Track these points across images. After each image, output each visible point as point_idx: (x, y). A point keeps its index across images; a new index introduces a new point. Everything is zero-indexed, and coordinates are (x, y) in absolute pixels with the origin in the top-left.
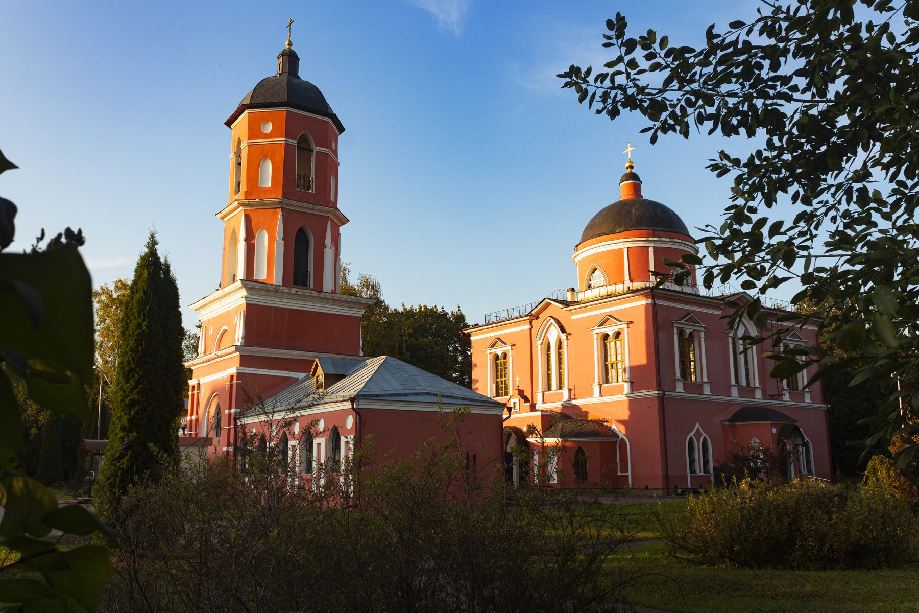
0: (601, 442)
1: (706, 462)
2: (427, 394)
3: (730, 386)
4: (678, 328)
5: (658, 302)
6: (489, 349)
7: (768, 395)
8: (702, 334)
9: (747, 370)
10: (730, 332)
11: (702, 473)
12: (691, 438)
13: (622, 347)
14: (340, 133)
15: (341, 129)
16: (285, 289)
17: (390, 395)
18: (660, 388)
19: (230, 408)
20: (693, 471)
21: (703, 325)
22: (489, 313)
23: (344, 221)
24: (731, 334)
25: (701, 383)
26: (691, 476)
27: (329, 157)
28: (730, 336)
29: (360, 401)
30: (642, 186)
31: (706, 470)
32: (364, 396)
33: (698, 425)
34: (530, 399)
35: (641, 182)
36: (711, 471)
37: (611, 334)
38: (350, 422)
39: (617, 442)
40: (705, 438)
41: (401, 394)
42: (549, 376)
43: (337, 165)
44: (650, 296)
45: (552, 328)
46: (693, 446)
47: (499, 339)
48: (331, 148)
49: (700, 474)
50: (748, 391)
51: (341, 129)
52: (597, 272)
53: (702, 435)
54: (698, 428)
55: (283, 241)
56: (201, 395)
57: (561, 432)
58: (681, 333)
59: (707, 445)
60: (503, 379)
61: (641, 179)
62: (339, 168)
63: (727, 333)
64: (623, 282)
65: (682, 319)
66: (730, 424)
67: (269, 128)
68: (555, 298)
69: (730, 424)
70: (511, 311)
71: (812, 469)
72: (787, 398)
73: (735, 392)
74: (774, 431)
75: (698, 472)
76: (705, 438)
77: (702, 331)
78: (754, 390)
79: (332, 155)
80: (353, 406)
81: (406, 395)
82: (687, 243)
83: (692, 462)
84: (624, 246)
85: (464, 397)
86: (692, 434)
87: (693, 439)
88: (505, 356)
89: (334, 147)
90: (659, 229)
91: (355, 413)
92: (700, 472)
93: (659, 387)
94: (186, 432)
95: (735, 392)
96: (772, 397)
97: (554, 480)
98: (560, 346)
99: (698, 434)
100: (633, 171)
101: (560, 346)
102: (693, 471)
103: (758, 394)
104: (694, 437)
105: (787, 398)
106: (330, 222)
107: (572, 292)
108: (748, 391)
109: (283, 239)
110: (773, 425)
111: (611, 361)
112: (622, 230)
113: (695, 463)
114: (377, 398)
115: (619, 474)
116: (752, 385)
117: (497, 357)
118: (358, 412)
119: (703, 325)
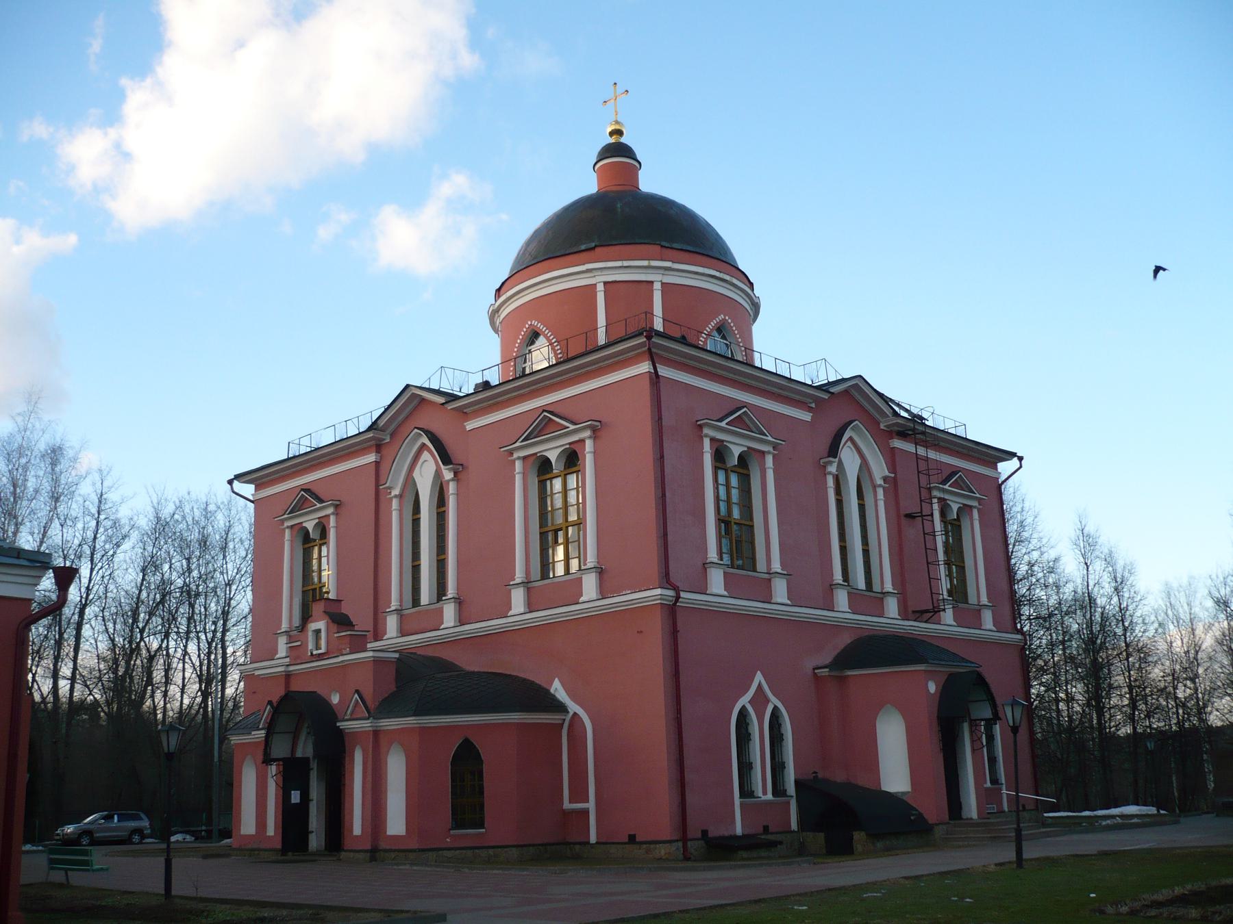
0: (521, 726)
1: (778, 768)
3: (832, 587)
4: (713, 440)
5: (664, 371)
6: (286, 516)
7: (910, 610)
8: (769, 461)
9: (866, 552)
10: (831, 463)
11: (770, 796)
12: (744, 708)
13: (581, 488)
18: (668, 582)
20: (746, 792)
21: (770, 438)
22: (294, 437)
24: (833, 469)
25: (766, 576)
26: (741, 804)
28: (830, 473)
31: (778, 790)
33: (759, 677)
35: (640, 163)
36: (791, 789)
37: (553, 456)
40: (775, 708)
42: (416, 569)
44: (647, 355)
45: (426, 455)
46: (747, 729)
47: (306, 490)
49: (764, 798)
50: (868, 600)
52: (541, 341)
53: (768, 701)
54: (760, 686)
58: (720, 455)
59: (780, 725)
63: (825, 467)
65: (721, 420)
66: (833, 674)
69: (833, 674)
71: (998, 777)
72: (948, 616)
73: (842, 599)
74: (932, 687)
75: (760, 794)
76: (775, 708)
77: (769, 452)
78: (882, 599)
82: (735, 281)
83: (745, 767)
84: (599, 280)
86: (744, 700)
87: (743, 468)
90: (675, 245)
92: (765, 793)
93: (666, 580)
95: (842, 599)
96: (919, 615)
97: (396, 824)
98: (441, 501)
99: (760, 700)
100: (623, 140)
101: (441, 501)
102: (746, 792)
103: (892, 606)
104: (750, 709)
105: (948, 616)
108: (868, 600)
110: (930, 675)
111: (552, 524)
112: (593, 245)
113: (753, 773)
115: (567, 805)
116: (877, 588)
119: (770, 438)
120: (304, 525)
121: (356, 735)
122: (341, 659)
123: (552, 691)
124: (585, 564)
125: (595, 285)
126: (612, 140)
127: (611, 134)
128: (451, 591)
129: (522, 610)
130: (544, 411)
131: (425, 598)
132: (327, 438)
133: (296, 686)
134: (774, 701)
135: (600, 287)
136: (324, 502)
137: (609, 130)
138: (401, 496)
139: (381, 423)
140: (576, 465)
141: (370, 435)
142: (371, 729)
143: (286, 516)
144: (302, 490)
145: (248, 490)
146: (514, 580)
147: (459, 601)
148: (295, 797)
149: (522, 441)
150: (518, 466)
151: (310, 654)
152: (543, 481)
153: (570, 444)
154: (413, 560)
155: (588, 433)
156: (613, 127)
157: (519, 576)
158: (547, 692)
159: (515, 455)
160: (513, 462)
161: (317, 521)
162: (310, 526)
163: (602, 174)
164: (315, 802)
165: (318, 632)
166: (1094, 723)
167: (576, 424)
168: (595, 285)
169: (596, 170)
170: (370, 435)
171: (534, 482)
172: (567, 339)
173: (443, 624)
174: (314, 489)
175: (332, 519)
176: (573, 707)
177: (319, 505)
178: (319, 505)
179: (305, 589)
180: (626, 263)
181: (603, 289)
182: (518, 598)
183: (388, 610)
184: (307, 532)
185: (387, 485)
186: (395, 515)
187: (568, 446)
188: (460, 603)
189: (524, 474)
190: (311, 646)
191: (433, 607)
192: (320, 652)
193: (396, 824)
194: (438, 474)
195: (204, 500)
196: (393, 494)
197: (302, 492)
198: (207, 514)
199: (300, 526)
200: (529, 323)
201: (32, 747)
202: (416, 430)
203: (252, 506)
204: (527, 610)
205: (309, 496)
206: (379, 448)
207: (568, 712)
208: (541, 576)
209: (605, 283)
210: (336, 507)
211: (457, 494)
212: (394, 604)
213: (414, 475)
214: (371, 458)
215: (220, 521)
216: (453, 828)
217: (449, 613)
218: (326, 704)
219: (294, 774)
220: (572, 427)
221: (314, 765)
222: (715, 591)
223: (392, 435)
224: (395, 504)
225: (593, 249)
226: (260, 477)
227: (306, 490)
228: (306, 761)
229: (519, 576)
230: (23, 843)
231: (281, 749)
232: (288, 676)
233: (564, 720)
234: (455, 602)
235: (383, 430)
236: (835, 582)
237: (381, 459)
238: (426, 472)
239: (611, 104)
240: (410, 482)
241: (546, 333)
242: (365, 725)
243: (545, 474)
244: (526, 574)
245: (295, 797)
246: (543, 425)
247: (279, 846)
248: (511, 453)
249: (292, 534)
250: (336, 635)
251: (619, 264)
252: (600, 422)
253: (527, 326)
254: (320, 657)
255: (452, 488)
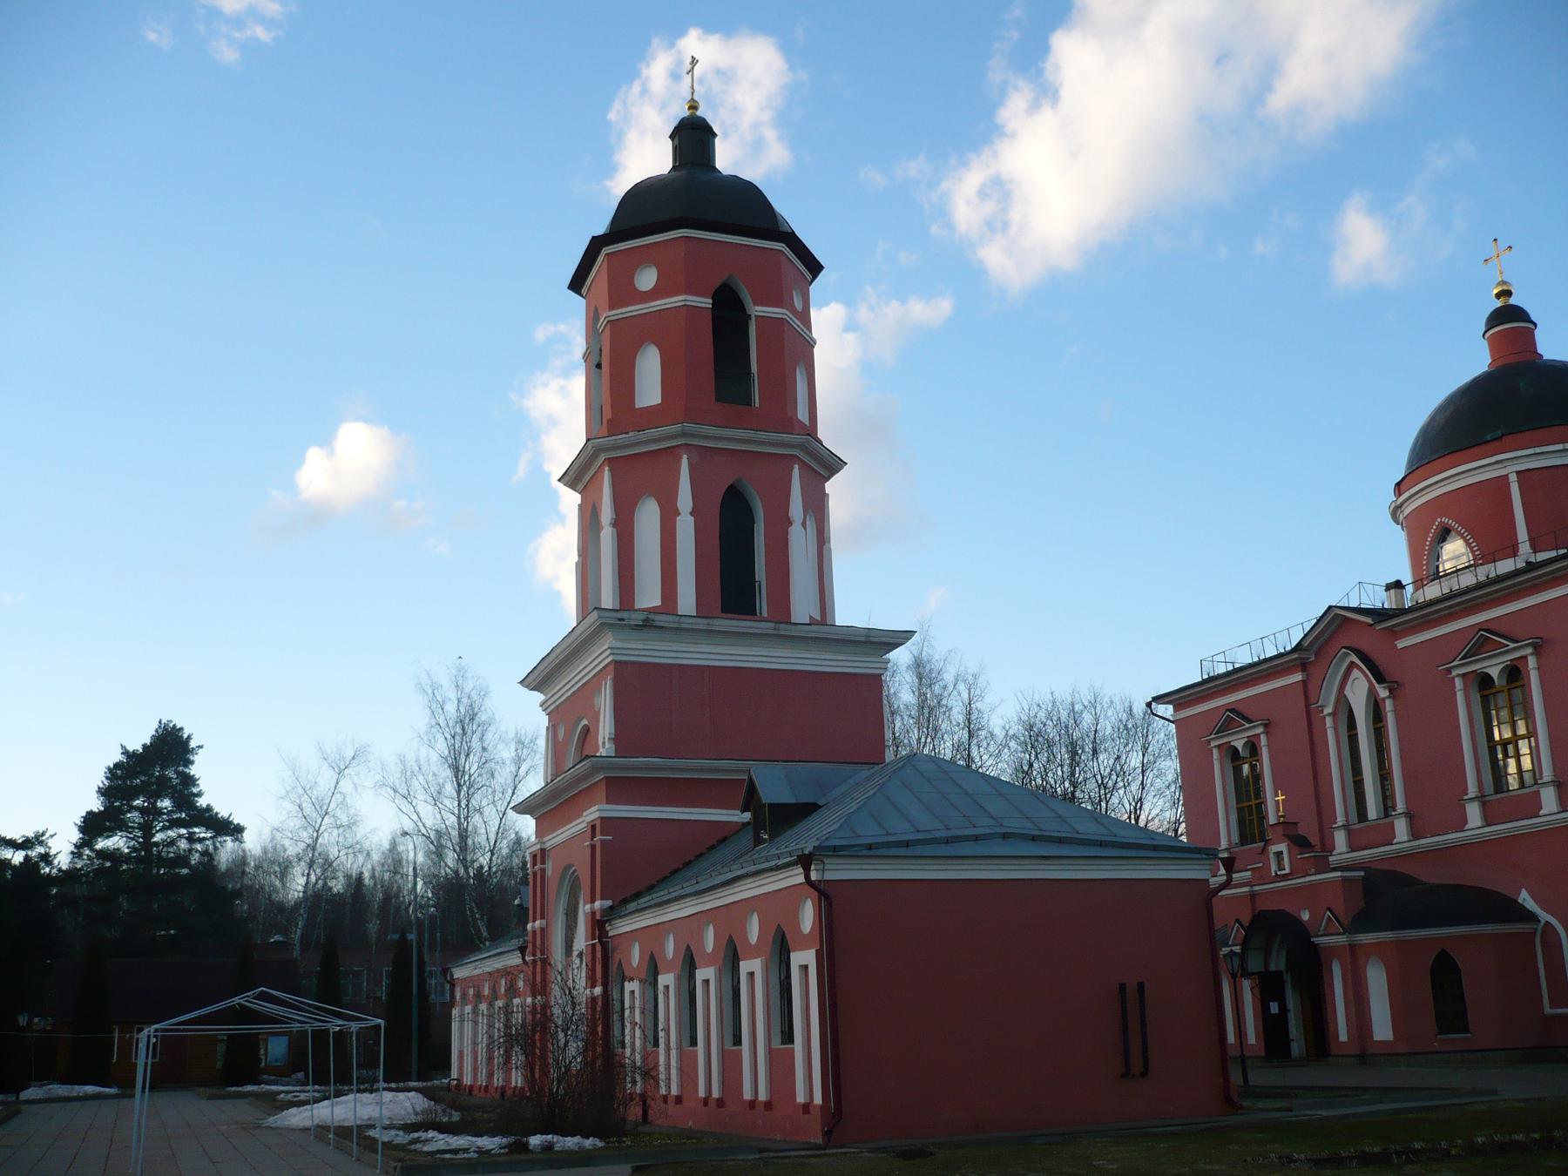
2: (1005, 836)
6: (1213, 736)
14: (815, 276)
15: (815, 267)
16: (702, 624)
17: (907, 844)
19: (593, 901)
22: (1207, 654)
23: (833, 465)
27: (786, 325)
29: (826, 861)
30: (1538, 334)
32: (835, 848)
34: (1315, 840)
35: (1535, 325)
37: (1494, 673)
38: (808, 917)
39: (1534, 933)
41: (936, 838)
43: (810, 344)
45: (1356, 673)
47: (1232, 711)
48: (793, 310)
51: (815, 267)
55: (693, 518)
56: (549, 872)
57: (459, 828)
60: (1253, 802)
61: (1534, 318)
62: (816, 350)
64: (1514, 553)
67: (647, 279)
68: (1354, 604)
70: (1257, 646)
79: (796, 322)
80: (807, 877)
81: (948, 841)
85: (1103, 838)
88: (1253, 747)
89: (798, 304)
91: (816, 893)
94: (527, 958)
97: (1382, 1029)
100: (1513, 301)
106: (796, 466)
107: (1398, 591)
109: (691, 514)
112: (1499, 433)
114: (908, 852)
115: (1548, 1010)
117: (1234, 755)
118: (824, 893)
120: (1232, 744)
121: (1333, 951)
122: (1308, 879)
123: (1520, 901)
124: (1542, 778)
125: (1507, 475)
126: (1499, 303)
127: (1498, 296)
128: (1400, 806)
129: (1479, 824)
130: (1481, 630)
131: (1372, 813)
132: (1244, 658)
133: (1263, 906)
135: (1513, 478)
136: (1252, 722)
137: (1495, 291)
138: (1334, 714)
139: (1306, 644)
140: (1517, 680)
141: (1295, 656)
142: (1346, 943)
143: (1213, 736)
144: (1228, 710)
145: (1166, 710)
146: (1467, 794)
147: (1410, 816)
148: (1274, 1008)
149: (1461, 660)
150: (1458, 683)
151: (1273, 874)
152: (1485, 696)
153: (1511, 660)
154: (1354, 776)
155: (1529, 650)
156: (1499, 289)
157: (1472, 790)
158: (1516, 902)
159: (1454, 673)
160: (1453, 679)
161: (1246, 740)
162: (1239, 745)
163: (1496, 344)
164: (1292, 1012)
165: (1279, 854)
166: (435, 1082)
167: (1517, 642)
168: (1506, 476)
169: (1486, 337)
170: (1295, 656)
171: (1476, 697)
172: (1493, 553)
173: (1395, 838)
174: (1240, 708)
175: (1263, 738)
176: (1545, 916)
177: (1247, 725)
178: (1247, 725)
179: (1240, 806)
180: (1538, 450)
181: (1516, 479)
182: (1474, 813)
183: (1334, 826)
185: (1319, 704)
186: (1330, 733)
187: (1509, 663)
188: (1410, 818)
189: (1466, 691)
190: (1274, 868)
191: (1381, 821)
192: (1283, 872)
193: (1382, 1029)
194: (1372, 692)
195: (1070, 700)
196: (1326, 712)
197: (1228, 713)
198: (1075, 716)
199: (1228, 745)
200: (1439, 520)
202: (1343, 650)
203: (1172, 726)
204: (1485, 824)
205: (1235, 717)
206: (1304, 666)
207: (1539, 921)
208: (1495, 790)
209: (1518, 473)
210: (1266, 726)
211: (1395, 711)
212: (1340, 820)
213: (666, 173)
215: (1087, 719)
216: (1439, 1034)
217: (1401, 828)
218: (1298, 921)
219: (1269, 987)
220: (1513, 645)
221: (1288, 978)
223: (1317, 654)
224: (1329, 721)
225: (1500, 438)
226: (1180, 698)
227: (1232, 711)
228: (1279, 974)
229: (1472, 790)
230: (722, 1098)
231: (1255, 964)
232: (1253, 896)
233: (1536, 929)
234: (1405, 817)
235: (1307, 649)
237: (1307, 678)
238: (1359, 690)
239: (1495, 262)
240: (1342, 701)
241: (1459, 529)
242: (1342, 939)
243: (1486, 689)
244: (1479, 788)
245: (1274, 1008)
246: (1482, 642)
247: (1263, 1054)
248: (1449, 671)
249: (1220, 755)
250: (1299, 857)
251: (1531, 451)
252: (1541, 638)
253: (1437, 523)
254: (1285, 877)
255: (1389, 705)
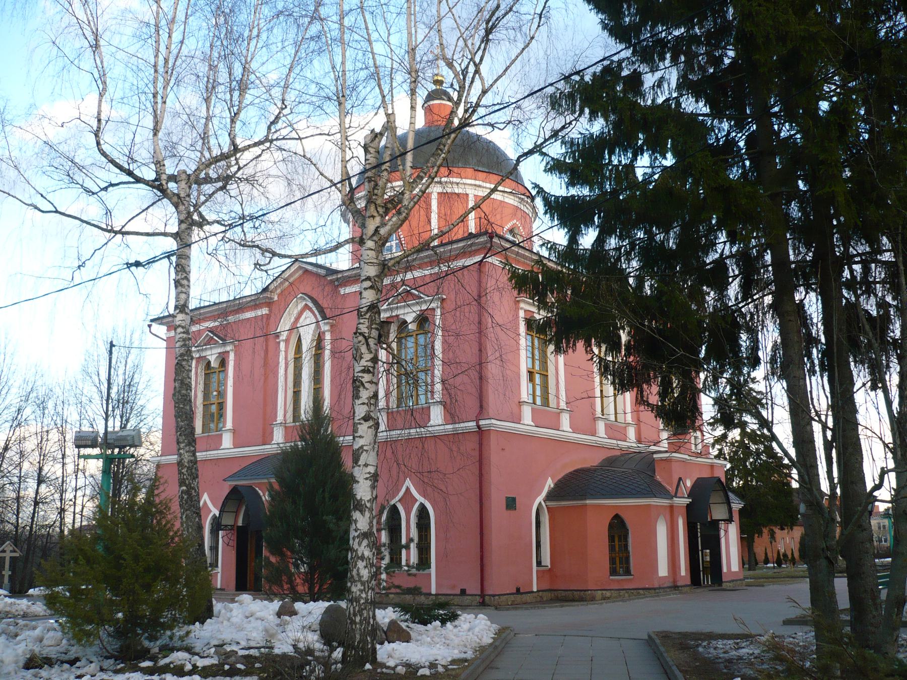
4: (525, 311)
33: (408, 483)
37: (409, 318)
95: (601, 427)
134: (421, 499)
139: (272, 287)
145: (161, 330)
184: (209, 363)
201: (538, 509)
203: (165, 343)
214: (265, 311)
222: (526, 422)
236: (597, 416)
255: (328, 336)
